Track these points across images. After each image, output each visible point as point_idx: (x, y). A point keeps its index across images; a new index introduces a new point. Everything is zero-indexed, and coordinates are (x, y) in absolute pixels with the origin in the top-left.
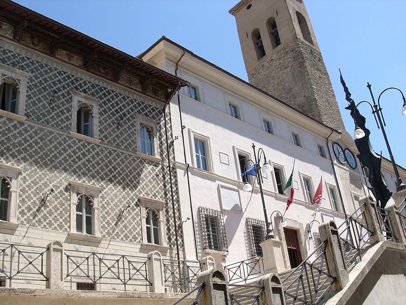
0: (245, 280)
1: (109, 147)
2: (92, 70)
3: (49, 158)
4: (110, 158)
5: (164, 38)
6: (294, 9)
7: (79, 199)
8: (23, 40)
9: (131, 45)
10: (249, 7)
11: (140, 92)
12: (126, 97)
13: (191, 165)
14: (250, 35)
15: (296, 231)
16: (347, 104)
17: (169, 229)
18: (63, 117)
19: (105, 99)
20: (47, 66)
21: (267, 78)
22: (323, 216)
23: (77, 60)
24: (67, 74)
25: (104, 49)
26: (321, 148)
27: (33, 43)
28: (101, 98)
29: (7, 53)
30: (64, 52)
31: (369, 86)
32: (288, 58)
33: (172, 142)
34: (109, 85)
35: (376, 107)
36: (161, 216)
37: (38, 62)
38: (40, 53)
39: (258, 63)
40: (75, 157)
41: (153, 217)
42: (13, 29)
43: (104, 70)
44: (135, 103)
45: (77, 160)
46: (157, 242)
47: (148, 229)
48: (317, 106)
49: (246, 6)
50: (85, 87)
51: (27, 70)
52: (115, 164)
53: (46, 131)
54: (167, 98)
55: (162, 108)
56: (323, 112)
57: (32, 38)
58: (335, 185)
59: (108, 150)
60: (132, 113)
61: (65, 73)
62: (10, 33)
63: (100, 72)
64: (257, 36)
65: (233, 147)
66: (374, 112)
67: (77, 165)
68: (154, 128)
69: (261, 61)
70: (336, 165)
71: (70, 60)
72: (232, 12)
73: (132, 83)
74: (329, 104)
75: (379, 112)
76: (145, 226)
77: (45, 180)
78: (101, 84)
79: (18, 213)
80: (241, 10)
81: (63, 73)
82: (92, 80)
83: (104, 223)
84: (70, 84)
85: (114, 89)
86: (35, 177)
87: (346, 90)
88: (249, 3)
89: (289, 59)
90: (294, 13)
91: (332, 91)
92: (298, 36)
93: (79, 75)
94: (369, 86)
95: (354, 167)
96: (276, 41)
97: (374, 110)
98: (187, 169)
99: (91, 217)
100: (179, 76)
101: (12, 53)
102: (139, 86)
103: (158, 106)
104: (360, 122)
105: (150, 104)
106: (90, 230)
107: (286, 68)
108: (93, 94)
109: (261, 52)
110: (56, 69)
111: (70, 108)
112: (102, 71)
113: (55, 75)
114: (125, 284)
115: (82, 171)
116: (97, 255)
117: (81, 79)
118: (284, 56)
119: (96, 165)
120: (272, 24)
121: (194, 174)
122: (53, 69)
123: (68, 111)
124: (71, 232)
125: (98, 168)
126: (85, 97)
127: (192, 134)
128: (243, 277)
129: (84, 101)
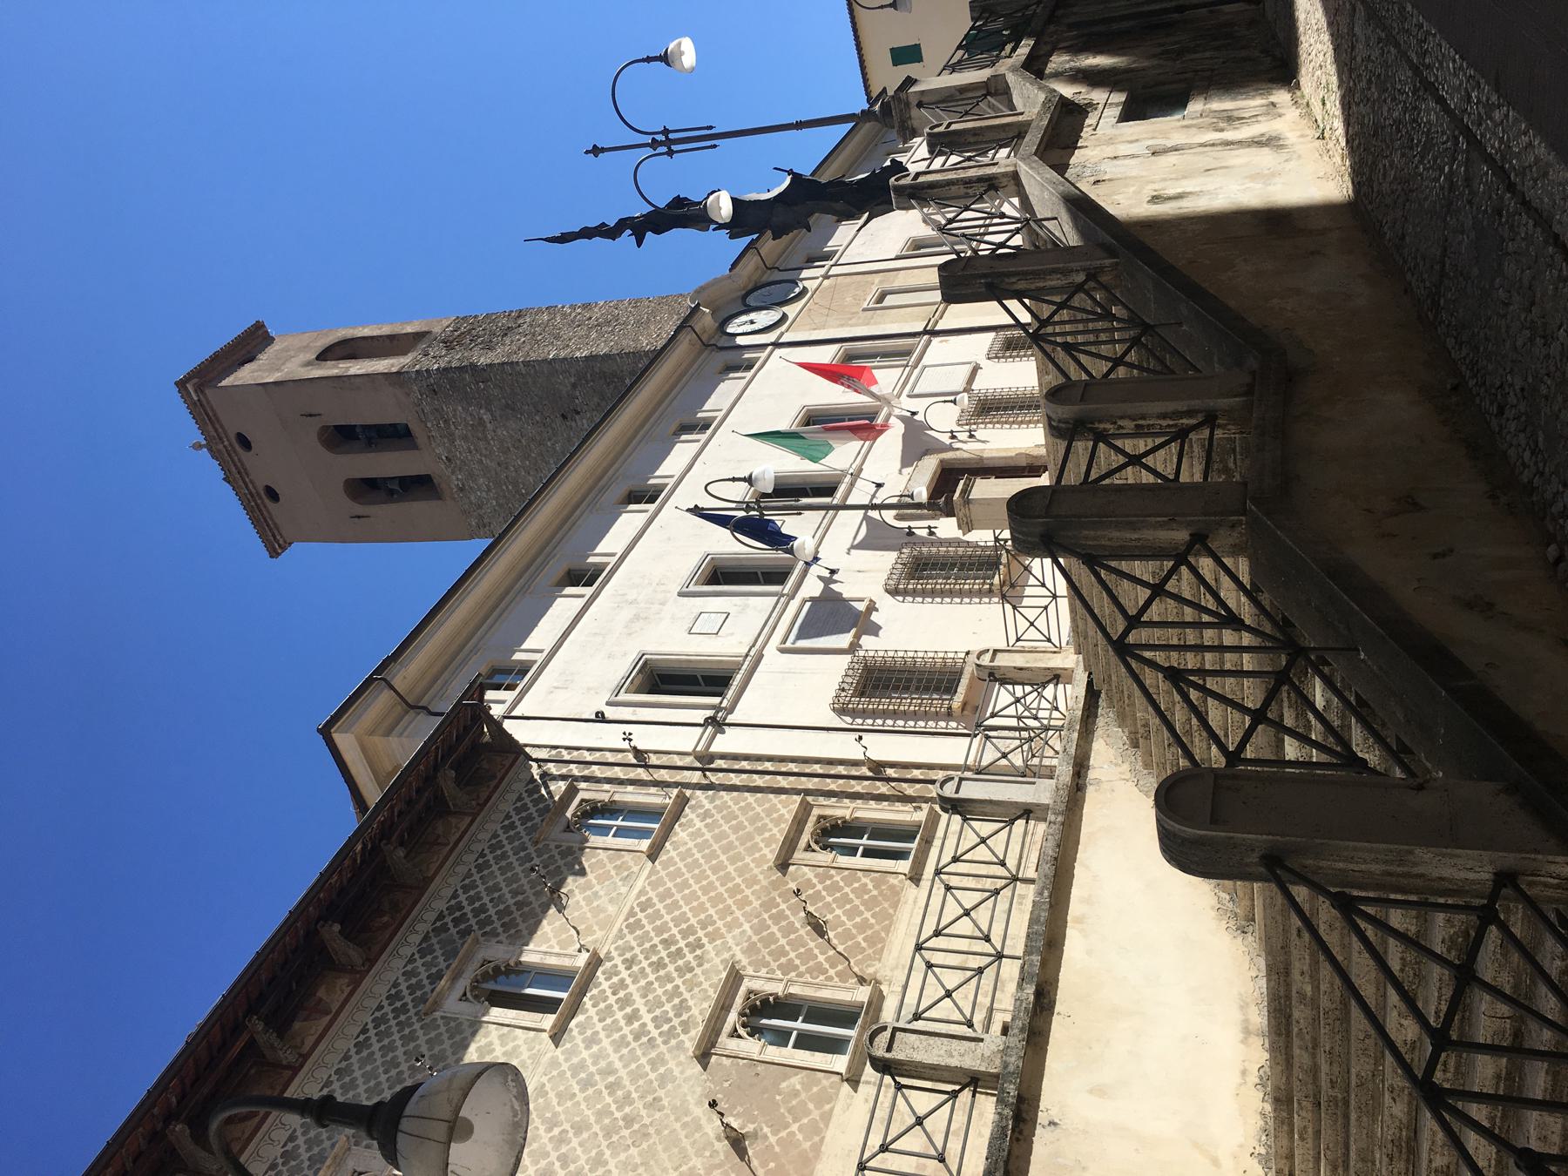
0: (1055, 596)
1: (617, 926)
3: (613, 1107)
4: (648, 928)
5: (326, 732)
6: (308, 364)
7: (751, 1035)
9: (322, 830)
10: (272, 494)
11: (472, 822)
12: (480, 861)
13: (710, 713)
14: (359, 509)
15: (943, 470)
16: (627, 238)
17: (880, 798)
19: (473, 922)
22: (916, 391)
23: (331, 992)
24: (370, 1026)
28: (468, 931)
30: (297, 1025)
31: (596, 151)
33: (638, 753)
34: (436, 902)
36: (839, 813)
40: (626, 1030)
41: (833, 834)
45: (636, 1025)
47: (869, 853)
48: (607, 357)
49: (267, 501)
50: (424, 975)
51: (327, 1144)
52: (667, 918)
53: (544, 1079)
56: (629, 345)
58: (836, 347)
59: (626, 931)
60: (531, 850)
61: (364, 1031)
64: (367, 489)
65: (681, 594)
66: (670, 153)
67: (651, 1026)
72: (275, 546)
75: (671, 136)
76: (858, 861)
77: (677, 1126)
78: (422, 928)
81: (362, 1038)
82: (407, 951)
84: (403, 1018)
85: (449, 892)
87: (587, 233)
92: (394, 370)
93: (382, 990)
94: (596, 151)
96: (395, 435)
97: (665, 149)
98: (717, 724)
102: (453, 820)
104: (684, 214)
105: (515, 796)
107: (481, 422)
108: (450, 955)
109: (419, 486)
110: (346, 1057)
112: (386, 919)
113: (363, 1063)
114: (1000, 956)
115: (671, 1014)
117: (396, 985)
119: (662, 973)
120: (343, 437)
121: (731, 710)
122: (344, 1064)
124: (843, 1070)
125: (671, 968)
126: (455, 978)
127: (623, 697)
128: (1045, 602)
129: (464, 983)
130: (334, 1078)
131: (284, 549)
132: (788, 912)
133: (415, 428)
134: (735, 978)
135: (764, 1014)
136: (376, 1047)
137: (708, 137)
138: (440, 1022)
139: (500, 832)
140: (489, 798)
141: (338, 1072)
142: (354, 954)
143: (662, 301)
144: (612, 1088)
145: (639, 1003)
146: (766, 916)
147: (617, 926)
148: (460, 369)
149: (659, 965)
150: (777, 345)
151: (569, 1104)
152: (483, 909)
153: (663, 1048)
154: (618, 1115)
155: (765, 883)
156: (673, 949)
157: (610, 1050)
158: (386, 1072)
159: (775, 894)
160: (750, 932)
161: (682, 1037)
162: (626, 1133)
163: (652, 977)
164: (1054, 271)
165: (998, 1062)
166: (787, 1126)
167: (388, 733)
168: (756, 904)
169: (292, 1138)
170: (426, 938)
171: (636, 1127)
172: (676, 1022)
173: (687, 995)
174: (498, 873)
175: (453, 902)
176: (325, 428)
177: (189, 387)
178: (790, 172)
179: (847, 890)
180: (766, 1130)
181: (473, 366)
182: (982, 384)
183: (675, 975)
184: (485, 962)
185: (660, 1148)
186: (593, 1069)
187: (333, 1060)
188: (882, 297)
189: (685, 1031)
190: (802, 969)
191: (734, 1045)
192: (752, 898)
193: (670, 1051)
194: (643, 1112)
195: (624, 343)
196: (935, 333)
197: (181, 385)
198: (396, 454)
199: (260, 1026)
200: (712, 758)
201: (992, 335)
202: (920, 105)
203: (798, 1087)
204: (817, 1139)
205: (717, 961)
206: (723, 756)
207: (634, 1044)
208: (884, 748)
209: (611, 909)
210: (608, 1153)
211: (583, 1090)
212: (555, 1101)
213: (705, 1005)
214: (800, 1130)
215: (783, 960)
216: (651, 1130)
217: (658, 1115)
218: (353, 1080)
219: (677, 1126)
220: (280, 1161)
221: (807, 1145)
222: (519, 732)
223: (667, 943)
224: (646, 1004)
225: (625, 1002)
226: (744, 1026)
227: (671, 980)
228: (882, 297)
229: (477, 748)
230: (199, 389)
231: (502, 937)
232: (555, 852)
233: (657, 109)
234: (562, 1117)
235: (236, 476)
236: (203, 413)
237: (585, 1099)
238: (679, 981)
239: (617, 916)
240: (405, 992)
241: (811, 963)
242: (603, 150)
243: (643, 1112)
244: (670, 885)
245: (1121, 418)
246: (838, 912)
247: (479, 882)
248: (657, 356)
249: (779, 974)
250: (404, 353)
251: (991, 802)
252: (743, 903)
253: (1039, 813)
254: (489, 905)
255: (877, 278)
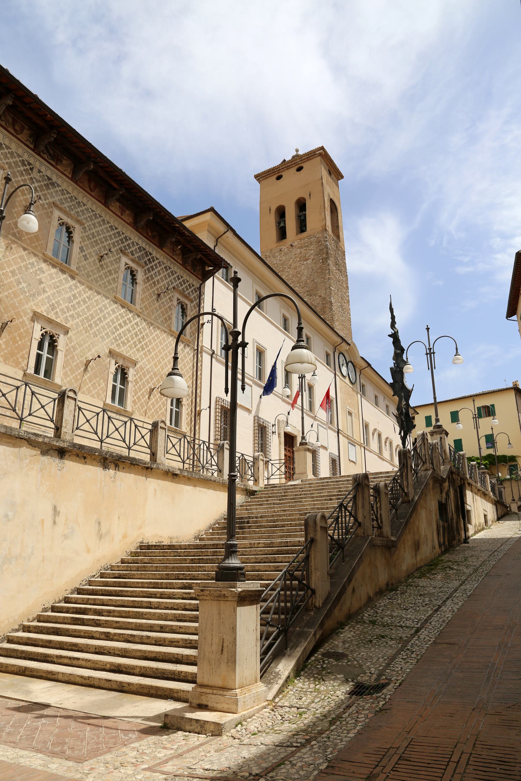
2: (188, 268)
5: (212, 210)
6: (329, 195)
7: (42, 335)
8: (81, 182)
16: (391, 331)
18: (110, 278)
20: (100, 216)
21: (283, 264)
23: (128, 217)
24: (117, 231)
25: (161, 212)
26: (328, 355)
27: (90, 187)
29: (65, 194)
30: (118, 204)
31: (428, 329)
32: (311, 250)
35: (430, 349)
37: (93, 211)
38: (97, 202)
39: (278, 244)
42: (72, 166)
43: (151, 232)
44: (129, 242)
46: (177, 425)
48: (331, 309)
54: (205, 276)
55: (199, 286)
56: (336, 318)
57: (89, 181)
62: (69, 170)
63: (148, 234)
64: (281, 213)
66: (427, 354)
67: (118, 332)
68: (189, 306)
69: (282, 243)
70: (339, 376)
71: (122, 215)
73: (174, 253)
74: (343, 310)
75: (432, 355)
76: (111, 383)
78: (147, 248)
79: (62, 375)
80: (268, 179)
81: (114, 228)
82: (140, 242)
83: (135, 398)
85: (158, 256)
86: (80, 339)
87: (393, 317)
88: (280, 174)
89: (312, 251)
90: (328, 200)
91: (348, 296)
92: (327, 228)
93: (128, 234)
94: (428, 329)
95: (353, 382)
96: (302, 227)
99: (42, 355)
100: (217, 251)
101: (70, 195)
102: (180, 257)
103: (195, 283)
105: (188, 279)
106: (122, 401)
109: (282, 234)
111: (117, 270)
112: (150, 234)
113: (106, 228)
116: (37, 395)
117: (130, 239)
118: (307, 246)
120: (301, 206)
122: (106, 222)
123: (116, 272)
129: (131, 264)
130: (102, 218)
131: (258, 180)
132: (153, 381)
133: (304, 234)
134: (135, 363)
135: (122, 374)
136: (111, 233)
137: (432, 367)
138: (119, 256)
139: (177, 275)
140: (187, 270)
141: (104, 220)
142: (142, 223)
143: (350, 330)
144: (100, 319)
145: (125, 328)
146: (152, 373)
147: (148, 319)
148: (327, 253)
149: (136, 335)
150: (335, 374)
151: (95, 304)
152: (153, 269)
153: (112, 337)
154: (92, 322)
155: (162, 373)
156: (141, 340)
157: (111, 318)
158: (104, 237)
159: (159, 377)
160: (147, 368)
161: (115, 344)
162: (87, 325)
163: (133, 332)
164: (408, 483)
165: (160, 462)
166: (90, 382)
167: (209, 231)
168: (155, 370)
169: (84, 205)
170: (144, 249)
171: (89, 328)
172: (120, 342)
173: (127, 345)
174: (164, 274)
175: (155, 258)
176: (305, 200)
177: (322, 151)
178: (412, 389)
179: (160, 403)
180: (89, 375)
181: (327, 258)
182: (321, 452)
183: (134, 341)
184: (137, 271)
185: (82, 337)
186: (105, 312)
187: (107, 218)
188: (350, 414)
189: (117, 345)
190: (136, 387)
191: (113, 362)
192: (157, 368)
193: (111, 339)
194: (93, 331)
195: (336, 316)
196: (338, 433)
197: (322, 148)
198: (295, 226)
199: (121, 193)
200: (201, 352)
201: (337, 455)
202: (441, 438)
203: (101, 386)
204: (87, 393)
205: (138, 356)
206: (202, 356)
207: (113, 326)
208: (205, 415)
209: (153, 317)
210: (81, 319)
211: (99, 309)
212: (96, 299)
213: (125, 352)
214: (89, 387)
215: (139, 380)
216: (88, 334)
217: (92, 336)
218: (101, 226)
219: (89, 343)
220: (77, 201)
221: (85, 389)
222: (209, 283)
223: (143, 337)
224: (125, 330)
225: (125, 323)
226: (119, 366)
227: (132, 339)
228: (350, 414)
229: (203, 264)
230: (320, 154)
231: (145, 277)
232: (171, 295)
233: (444, 351)
234: (91, 302)
235: (285, 165)
236: (311, 155)
237: (96, 310)
238: (132, 342)
239: (151, 319)
240: (127, 243)
241: (138, 390)
242: (428, 331)
243: (93, 331)
244: (161, 338)
245: (380, 504)
246: (154, 399)
247: (161, 267)
248: (332, 329)
249: (134, 378)
250: (333, 232)
251: (223, 459)
252: (155, 365)
253: (220, 474)
254: (154, 272)
255: (356, 411)
